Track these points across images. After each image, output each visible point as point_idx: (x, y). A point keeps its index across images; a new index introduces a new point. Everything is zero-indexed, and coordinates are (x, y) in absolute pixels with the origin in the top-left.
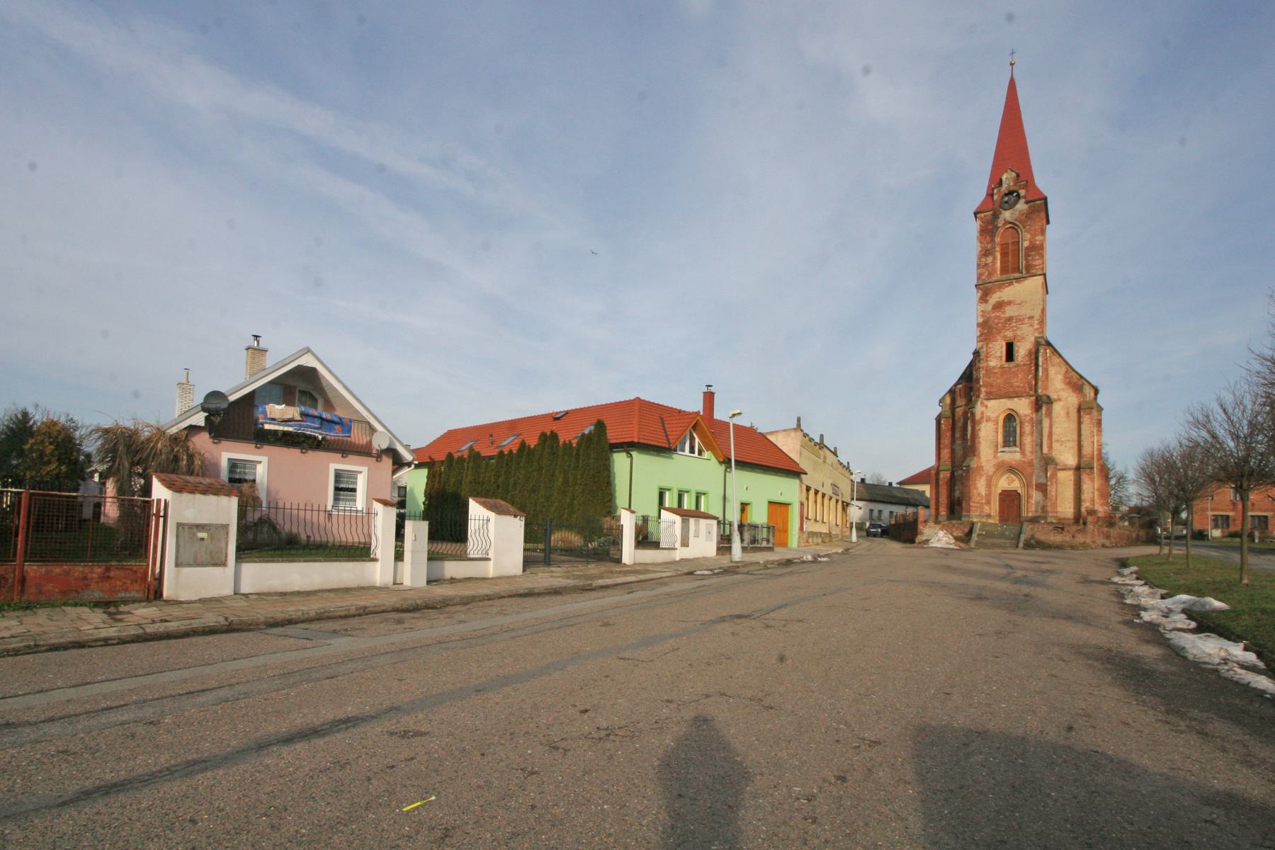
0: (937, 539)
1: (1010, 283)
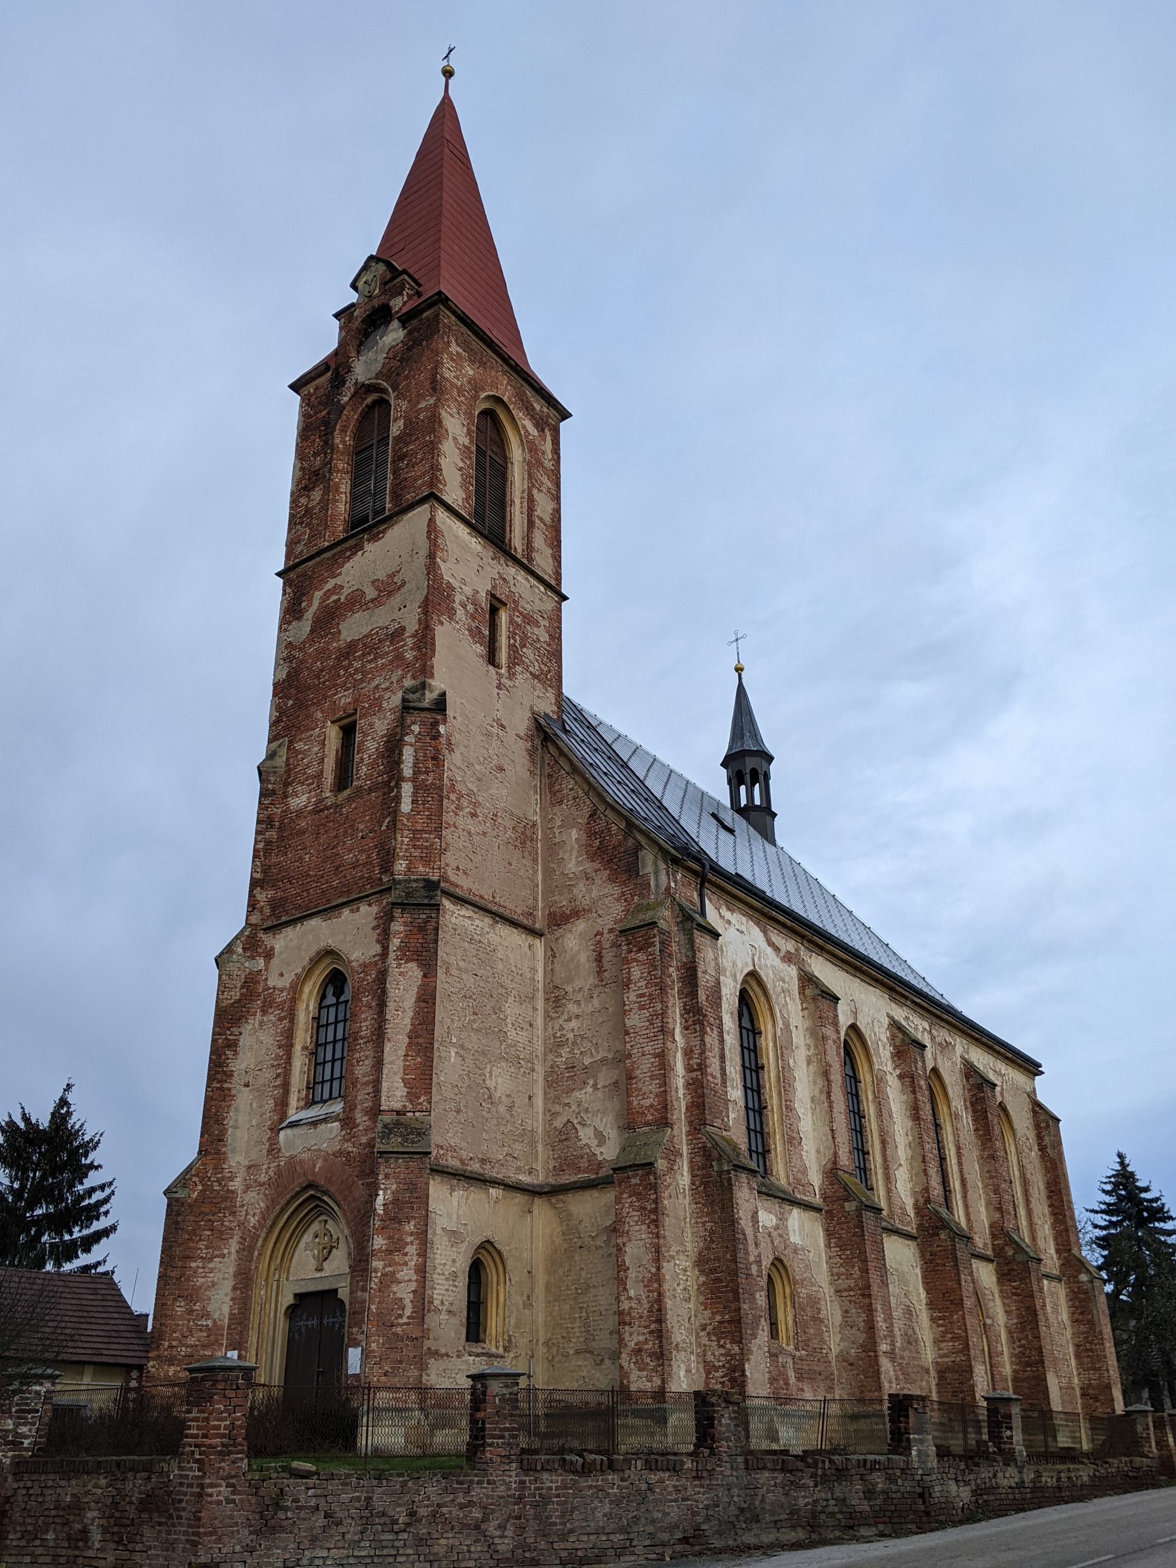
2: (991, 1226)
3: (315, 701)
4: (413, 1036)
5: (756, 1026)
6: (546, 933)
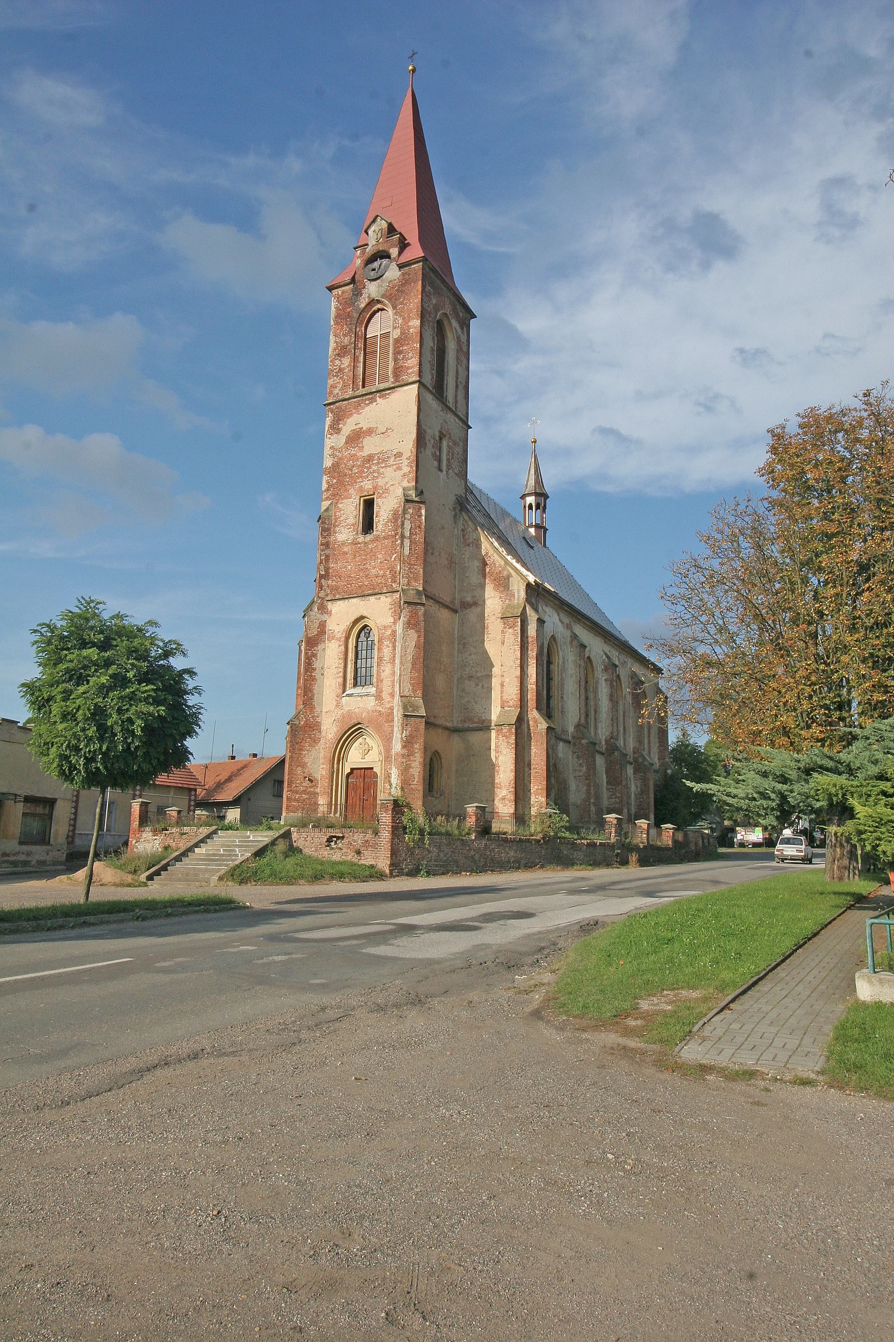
2: (634, 748)
3: (350, 483)
5: (551, 659)
6: (459, 611)
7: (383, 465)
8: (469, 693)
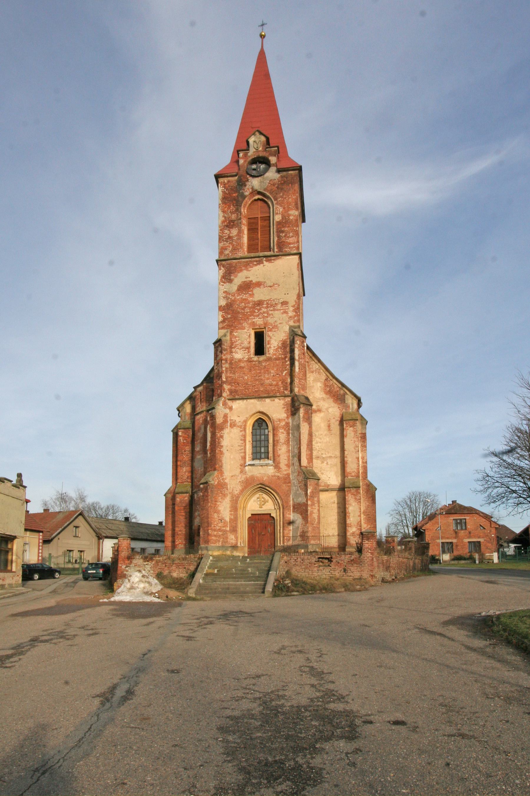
0: (128, 586)
1: (259, 261)
4: (308, 445)
7: (272, 309)
8: (317, 468)
